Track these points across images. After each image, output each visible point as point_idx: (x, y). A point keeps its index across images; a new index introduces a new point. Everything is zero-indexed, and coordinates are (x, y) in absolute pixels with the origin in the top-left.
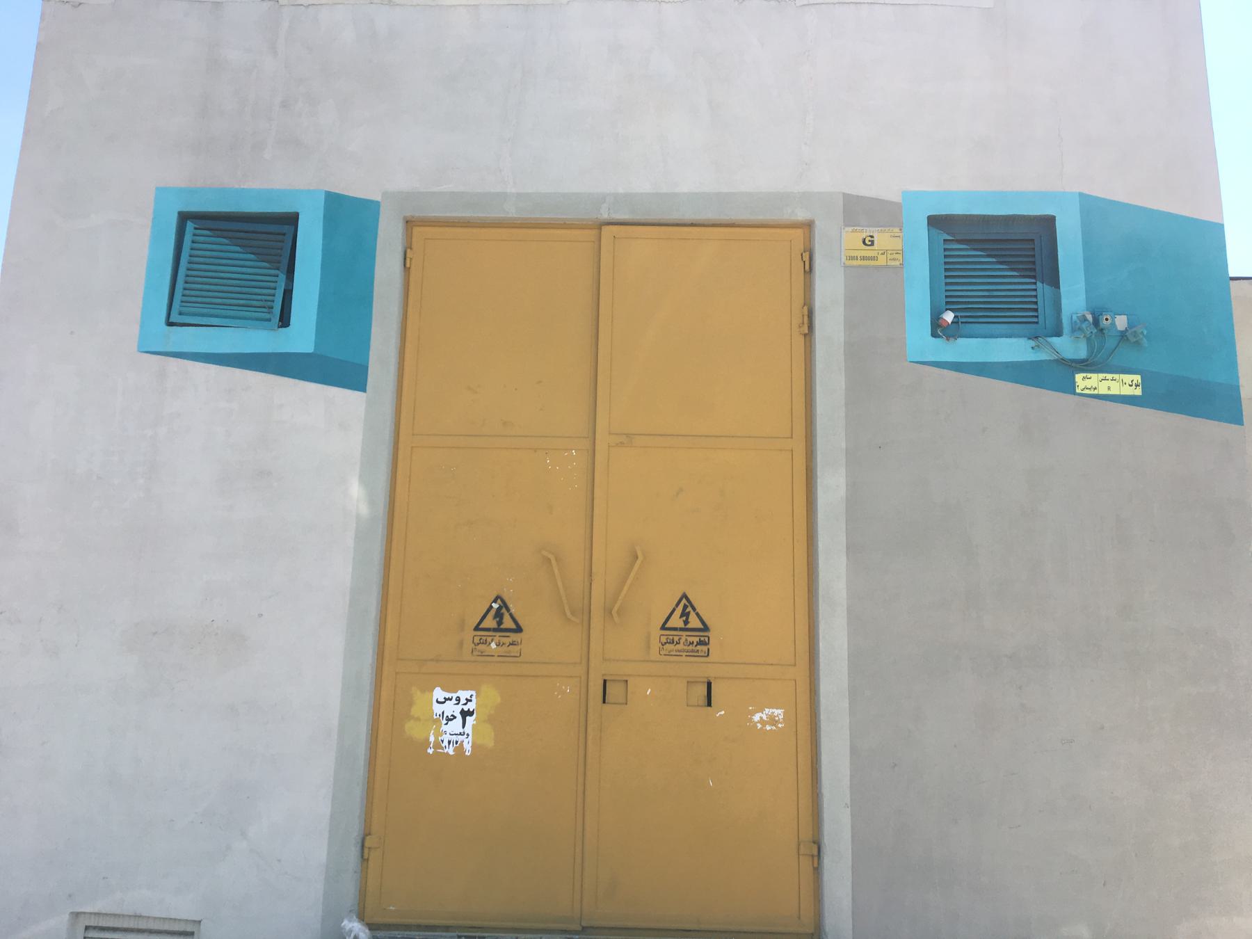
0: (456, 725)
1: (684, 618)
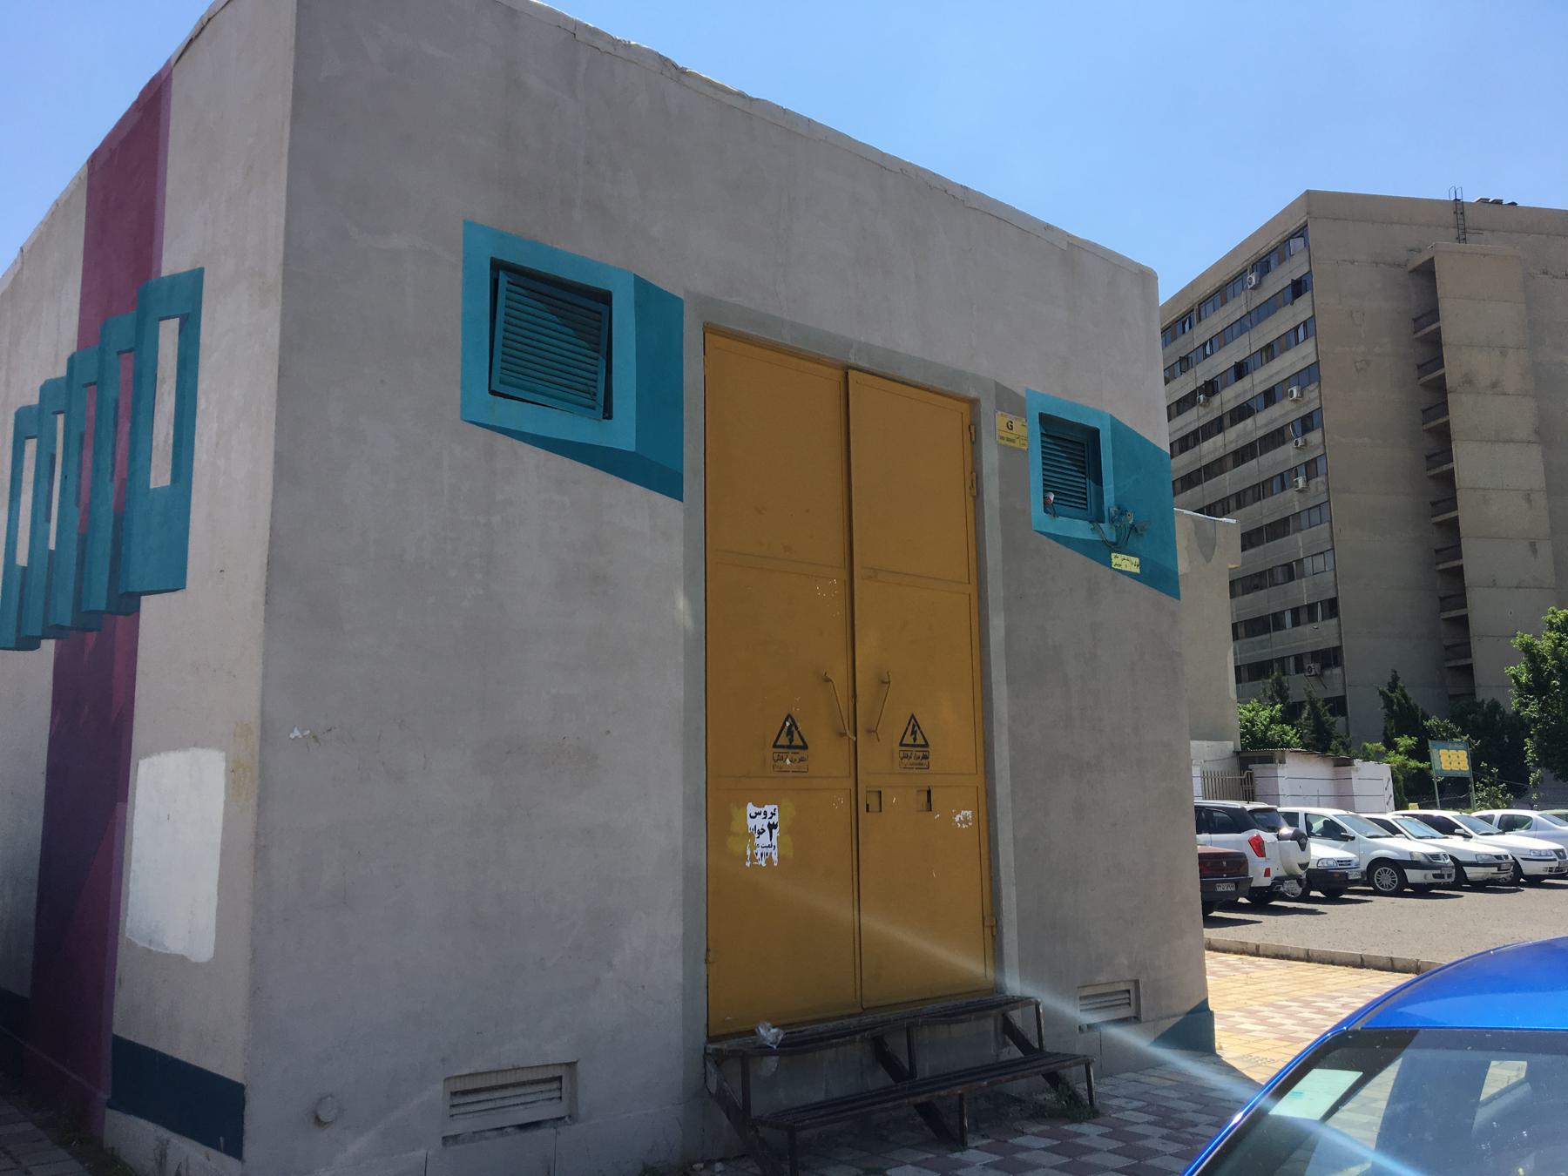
0: (764, 839)
1: (789, 737)
